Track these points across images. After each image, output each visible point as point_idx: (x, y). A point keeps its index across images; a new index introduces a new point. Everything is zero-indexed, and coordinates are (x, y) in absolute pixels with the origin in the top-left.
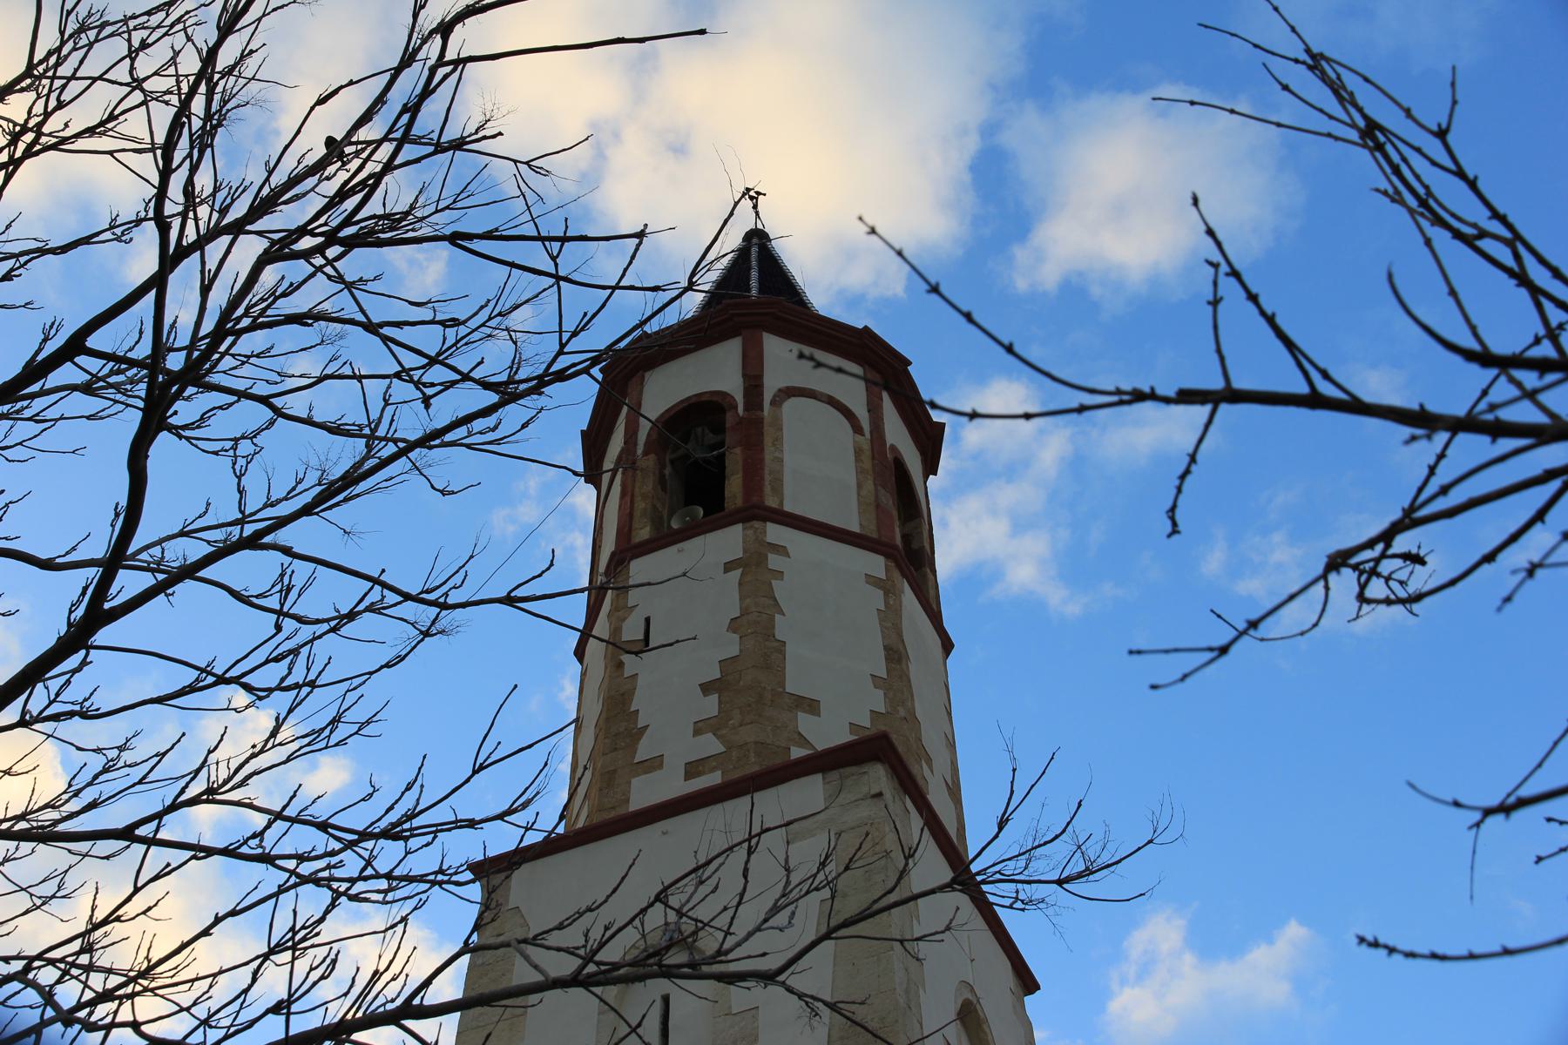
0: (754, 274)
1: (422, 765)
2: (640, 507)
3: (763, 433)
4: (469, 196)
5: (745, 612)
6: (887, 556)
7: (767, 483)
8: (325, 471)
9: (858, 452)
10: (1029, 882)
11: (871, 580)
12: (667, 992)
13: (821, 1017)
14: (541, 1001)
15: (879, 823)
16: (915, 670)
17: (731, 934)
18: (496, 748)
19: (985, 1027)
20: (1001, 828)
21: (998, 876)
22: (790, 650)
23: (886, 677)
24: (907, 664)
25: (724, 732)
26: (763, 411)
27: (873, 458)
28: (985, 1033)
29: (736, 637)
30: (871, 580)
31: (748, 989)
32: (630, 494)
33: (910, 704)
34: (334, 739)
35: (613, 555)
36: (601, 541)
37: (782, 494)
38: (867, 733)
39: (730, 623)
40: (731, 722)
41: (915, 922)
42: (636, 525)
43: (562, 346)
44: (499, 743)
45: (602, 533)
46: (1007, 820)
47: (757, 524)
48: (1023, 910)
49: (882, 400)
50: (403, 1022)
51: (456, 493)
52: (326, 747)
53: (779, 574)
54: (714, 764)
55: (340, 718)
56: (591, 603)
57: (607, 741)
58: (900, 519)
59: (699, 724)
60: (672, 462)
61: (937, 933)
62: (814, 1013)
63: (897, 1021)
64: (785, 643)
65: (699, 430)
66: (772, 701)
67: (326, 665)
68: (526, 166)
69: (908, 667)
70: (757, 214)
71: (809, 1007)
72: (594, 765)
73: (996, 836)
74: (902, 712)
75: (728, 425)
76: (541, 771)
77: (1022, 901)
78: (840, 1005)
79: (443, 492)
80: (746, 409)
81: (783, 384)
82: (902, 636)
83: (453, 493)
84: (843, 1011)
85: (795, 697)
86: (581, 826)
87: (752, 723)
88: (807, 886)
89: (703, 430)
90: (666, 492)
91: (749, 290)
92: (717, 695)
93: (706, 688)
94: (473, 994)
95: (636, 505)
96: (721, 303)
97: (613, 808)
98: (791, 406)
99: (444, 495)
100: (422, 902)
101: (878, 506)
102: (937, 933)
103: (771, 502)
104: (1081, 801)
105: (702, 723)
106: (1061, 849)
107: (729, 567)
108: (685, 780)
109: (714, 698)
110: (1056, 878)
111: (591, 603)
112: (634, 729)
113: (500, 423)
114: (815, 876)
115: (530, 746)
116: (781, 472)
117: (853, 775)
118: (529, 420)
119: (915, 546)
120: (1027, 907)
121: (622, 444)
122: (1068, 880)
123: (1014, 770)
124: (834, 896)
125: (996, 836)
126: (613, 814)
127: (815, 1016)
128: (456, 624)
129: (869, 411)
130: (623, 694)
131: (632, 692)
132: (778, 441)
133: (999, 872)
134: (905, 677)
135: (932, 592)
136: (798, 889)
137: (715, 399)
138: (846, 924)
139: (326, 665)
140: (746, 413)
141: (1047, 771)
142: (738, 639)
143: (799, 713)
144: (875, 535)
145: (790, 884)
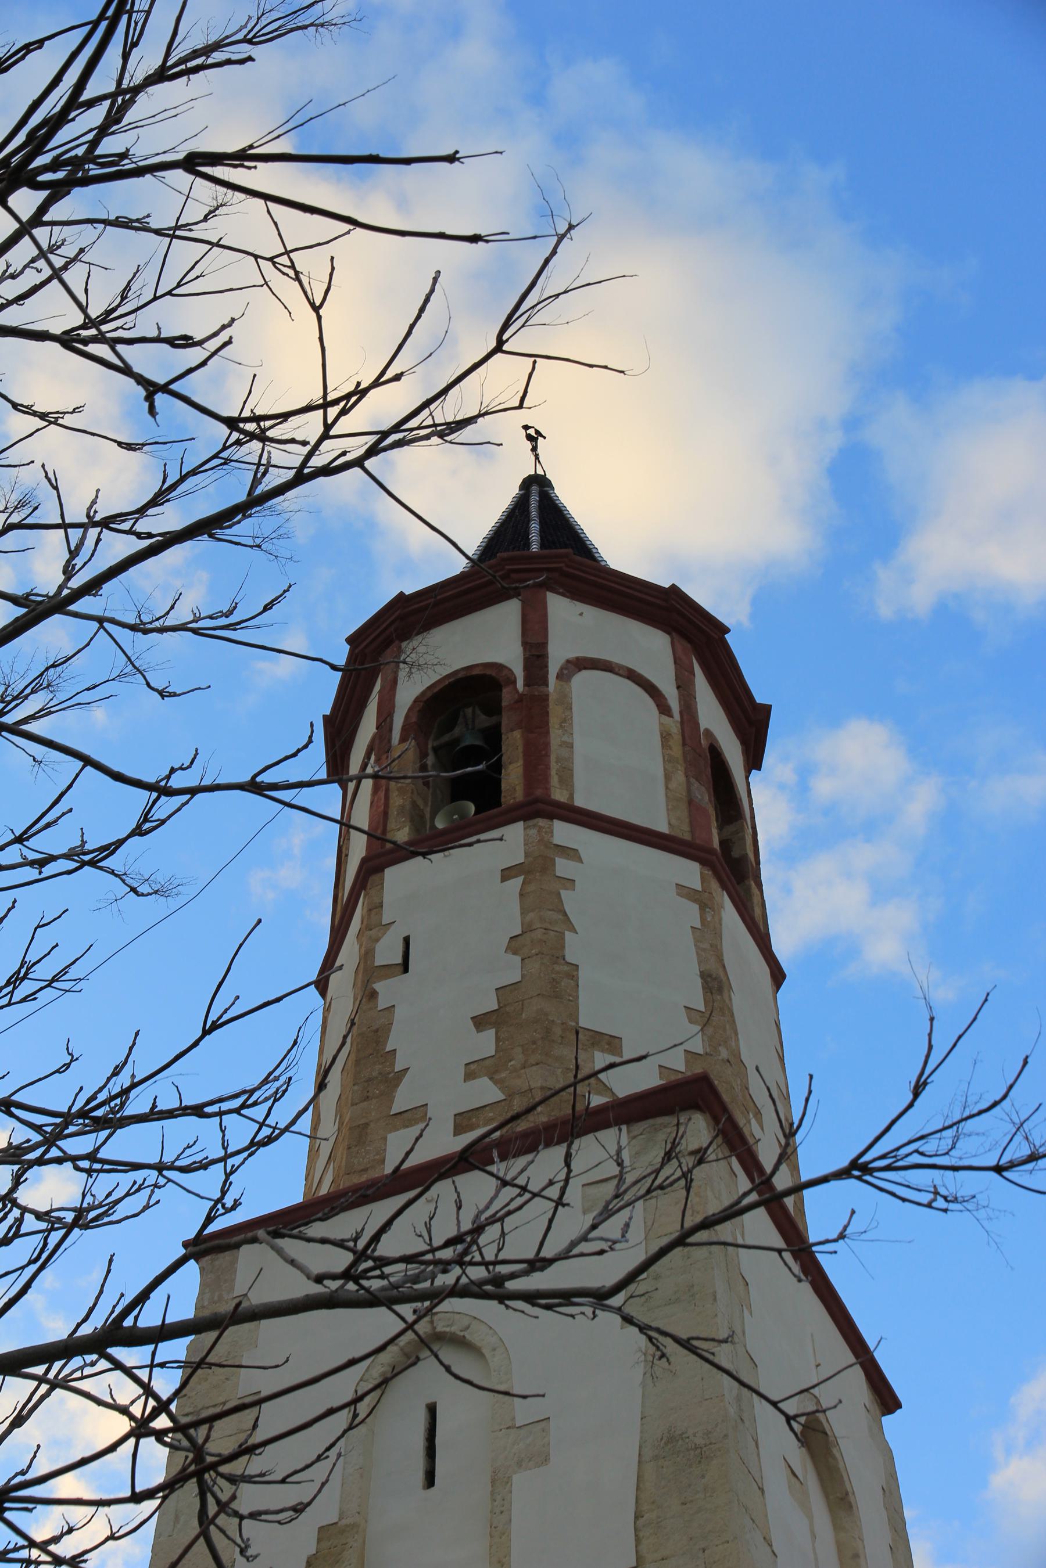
0: (535, 527)
1: (134, 1044)
2: (397, 804)
3: (548, 713)
4: (198, 277)
5: (527, 929)
6: (703, 862)
7: (553, 772)
8: (9, 686)
9: (665, 737)
10: (955, 1169)
11: (684, 891)
12: (433, 1401)
13: (668, 1360)
14: (287, 1361)
15: (700, 1187)
16: (739, 1002)
17: (564, 1205)
18: (233, 1004)
19: (835, 1451)
20: (916, 1094)
21: (916, 1159)
22: (584, 975)
23: (704, 1011)
24: (730, 997)
25: (503, 1075)
26: (547, 686)
27: (684, 744)
28: (834, 1458)
29: (517, 959)
30: (684, 891)
31: (573, 1316)
32: (384, 788)
33: (733, 1044)
34: (18, 995)
35: (364, 861)
36: (348, 849)
37: (573, 786)
38: (680, 1076)
39: (319, 1532)
40: (510, 1064)
41: (746, 1312)
42: (392, 824)
43: (328, 427)
44: (237, 998)
45: (349, 839)
46: (925, 1083)
47: (541, 822)
48: (945, 1211)
49: (694, 675)
50: (110, 1350)
51: (179, 695)
52: (9, 1004)
53: (570, 883)
54: (491, 1114)
55: (27, 973)
56: (336, 923)
57: (356, 1088)
58: (717, 821)
59: (473, 1067)
60: (435, 750)
61: (827, 1241)
62: (659, 1353)
63: (726, 1436)
64: (577, 966)
65: (469, 711)
66: (562, 1037)
67: (9, 910)
68: (270, 263)
69: (730, 999)
70: (537, 457)
71: (653, 1344)
72: (340, 1117)
73: (911, 1106)
74: (724, 1053)
75: (504, 704)
76: (289, 1051)
77: (945, 1198)
78: (695, 1343)
79: (162, 694)
80: (527, 684)
81: (572, 655)
82: (723, 960)
83: (174, 695)
84: (700, 1351)
85: (591, 1033)
86: (326, 1192)
87: (537, 1064)
88: (648, 1185)
89: (474, 712)
90: (428, 787)
91: (527, 544)
92: (494, 1030)
93: (480, 1022)
94: (206, 1313)
95: (391, 801)
96: (495, 556)
97: (365, 1170)
98: (582, 679)
99: (163, 697)
100: (136, 1187)
101: (690, 802)
102: (827, 1241)
103: (559, 795)
104: (1027, 1057)
105: (476, 1065)
106: (996, 1125)
107: (507, 874)
108: (454, 1136)
109: (490, 1034)
110: (993, 1163)
111: (336, 923)
112: (389, 1073)
113: (235, 608)
114: (657, 1172)
115: (278, 1000)
116: (570, 759)
117: (665, 1127)
118: (273, 601)
119: (736, 853)
120: (952, 1206)
121: (374, 730)
122: (1012, 1165)
123: (932, 1019)
124: (690, 1187)
125: (911, 1106)
126: (364, 1178)
127: (660, 1358)
128: (176, 883)
129: (678, 687)
130: (377, 1031)
131: (387, 1028)
132: (566, 723)
133: (917, 1151)
134: (727, 1010)
135: (757, 911)
136: (636, 1188)
137: (488, 672)
138: (707, 1224)
139: (9, 910)
140: (527, 688)
141: (978, 1017)
142: (520, 960)
143: (595, 1052)
144: (687, 837)
145: (624, 1182)
